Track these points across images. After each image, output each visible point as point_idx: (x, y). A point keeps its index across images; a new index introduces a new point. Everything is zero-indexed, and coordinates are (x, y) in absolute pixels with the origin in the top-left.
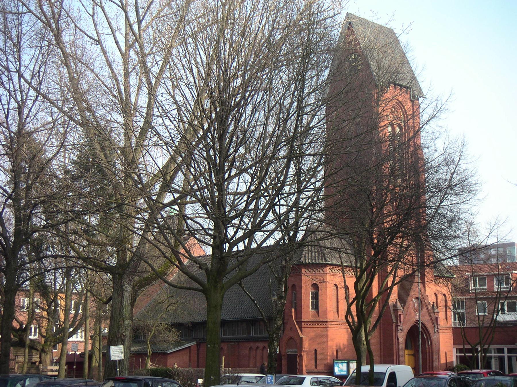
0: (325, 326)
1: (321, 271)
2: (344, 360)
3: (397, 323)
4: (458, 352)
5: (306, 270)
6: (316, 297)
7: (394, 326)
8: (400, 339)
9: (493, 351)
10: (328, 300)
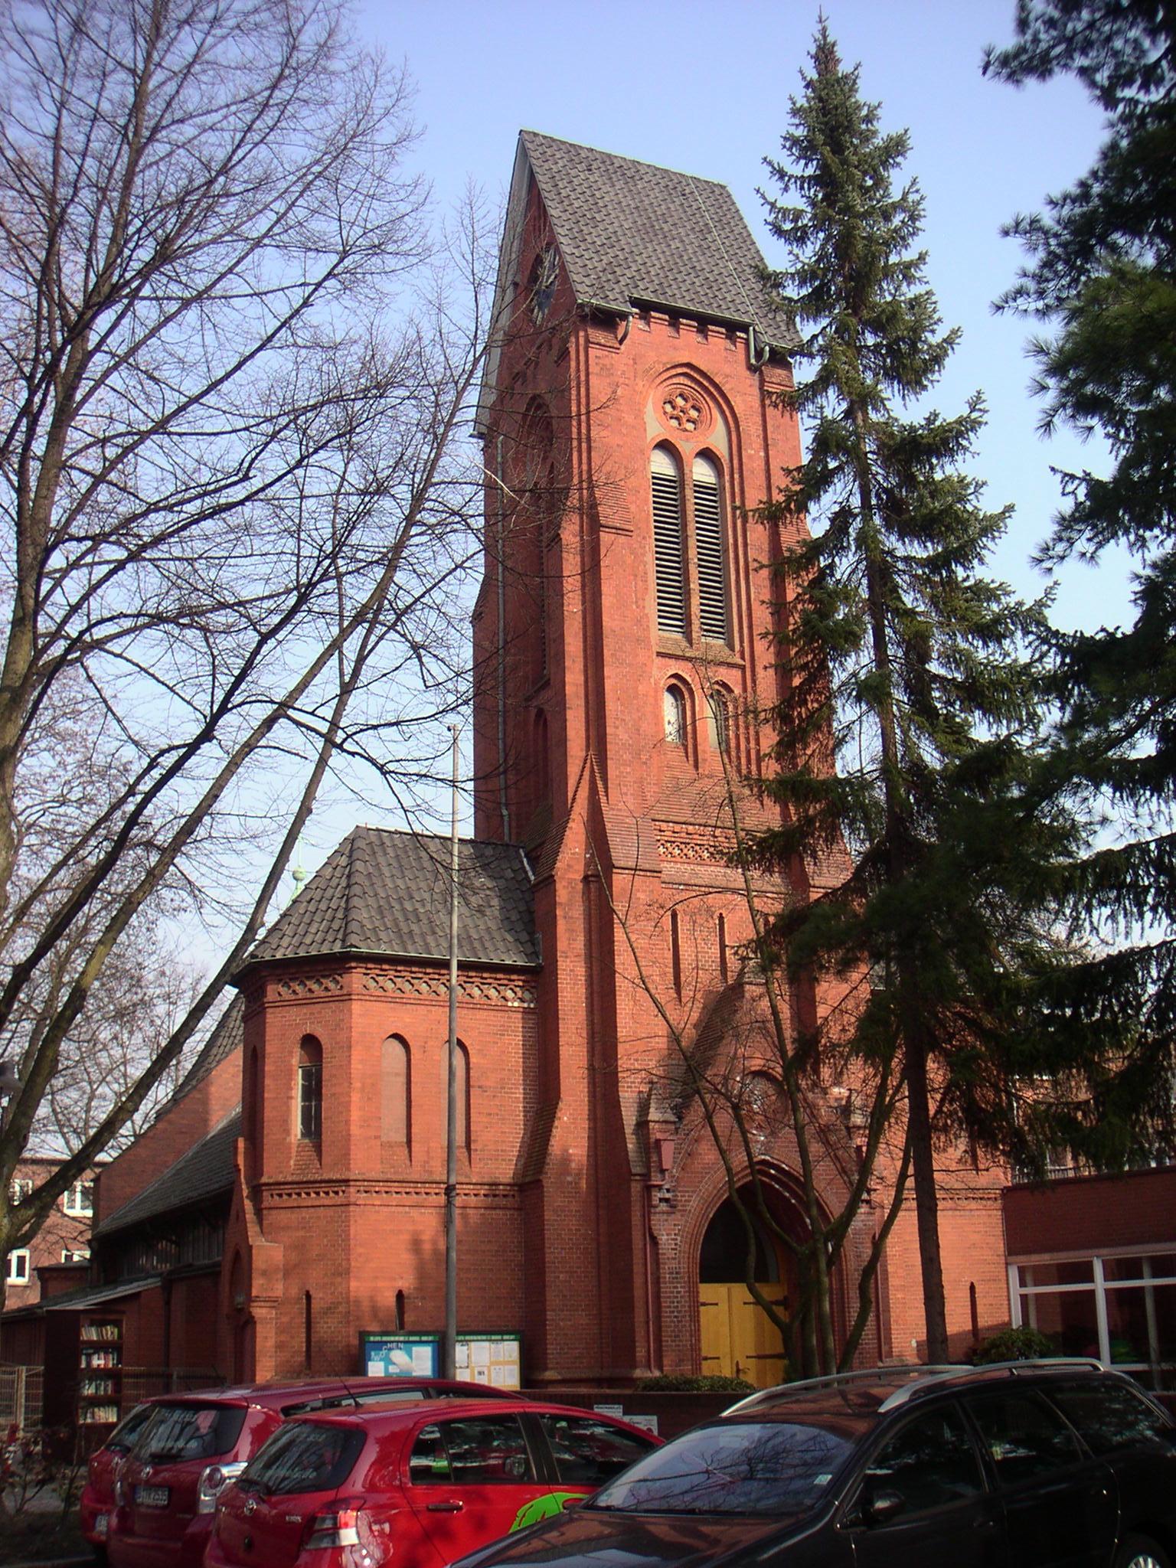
0: (340, 1199)
1: (332, 985)
2: (427, 1333)
3: (646, 1176)
4: (1029, 1279)
5: (283, 990)
6: (313, 1091)
7: (636, 1188)
8: (663, 1238)
9: (1146, 1270)
10: (355, 1097)
